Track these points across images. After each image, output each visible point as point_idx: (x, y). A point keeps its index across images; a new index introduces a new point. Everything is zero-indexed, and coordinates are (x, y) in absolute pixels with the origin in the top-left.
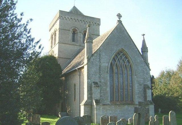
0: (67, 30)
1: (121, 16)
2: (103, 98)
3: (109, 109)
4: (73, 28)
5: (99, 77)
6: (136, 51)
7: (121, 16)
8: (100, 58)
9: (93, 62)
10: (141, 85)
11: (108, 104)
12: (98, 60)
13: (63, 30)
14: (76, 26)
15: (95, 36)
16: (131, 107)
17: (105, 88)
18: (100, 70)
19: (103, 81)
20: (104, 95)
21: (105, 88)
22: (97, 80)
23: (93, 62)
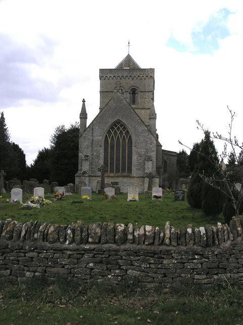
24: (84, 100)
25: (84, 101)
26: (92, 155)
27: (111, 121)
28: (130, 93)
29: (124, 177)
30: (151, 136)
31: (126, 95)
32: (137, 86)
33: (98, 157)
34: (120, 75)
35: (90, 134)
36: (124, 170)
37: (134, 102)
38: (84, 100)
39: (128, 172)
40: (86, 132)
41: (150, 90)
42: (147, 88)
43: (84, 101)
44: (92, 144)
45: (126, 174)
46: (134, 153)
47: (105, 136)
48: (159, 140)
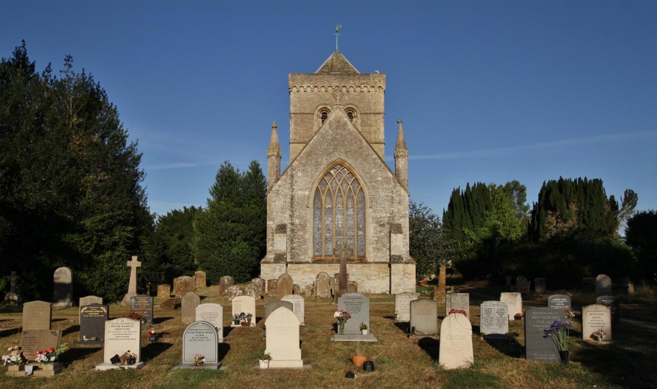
0: (307, 114)
1: (117, 356)
2: (298, 251)
3: (308, 270)
4: (320, 107)
5: (291, 216)
6: (374, 160)
7: (117, 356)
8: (292, 182)
9: (278, 191)
10: (383, 225)
11: (308, 263)
12: (288, 186)
13: (298, 116)
14: (327, 102)
15: (107, 308)
16: (356, 268)
17: (301, 233)
18: (292, 203)
19: (297, 221)
20: (300, 246)
21: (301, 233)
22: (287, 221)
23: (278, 191)
30: (399, 188)
32: (356, 103)
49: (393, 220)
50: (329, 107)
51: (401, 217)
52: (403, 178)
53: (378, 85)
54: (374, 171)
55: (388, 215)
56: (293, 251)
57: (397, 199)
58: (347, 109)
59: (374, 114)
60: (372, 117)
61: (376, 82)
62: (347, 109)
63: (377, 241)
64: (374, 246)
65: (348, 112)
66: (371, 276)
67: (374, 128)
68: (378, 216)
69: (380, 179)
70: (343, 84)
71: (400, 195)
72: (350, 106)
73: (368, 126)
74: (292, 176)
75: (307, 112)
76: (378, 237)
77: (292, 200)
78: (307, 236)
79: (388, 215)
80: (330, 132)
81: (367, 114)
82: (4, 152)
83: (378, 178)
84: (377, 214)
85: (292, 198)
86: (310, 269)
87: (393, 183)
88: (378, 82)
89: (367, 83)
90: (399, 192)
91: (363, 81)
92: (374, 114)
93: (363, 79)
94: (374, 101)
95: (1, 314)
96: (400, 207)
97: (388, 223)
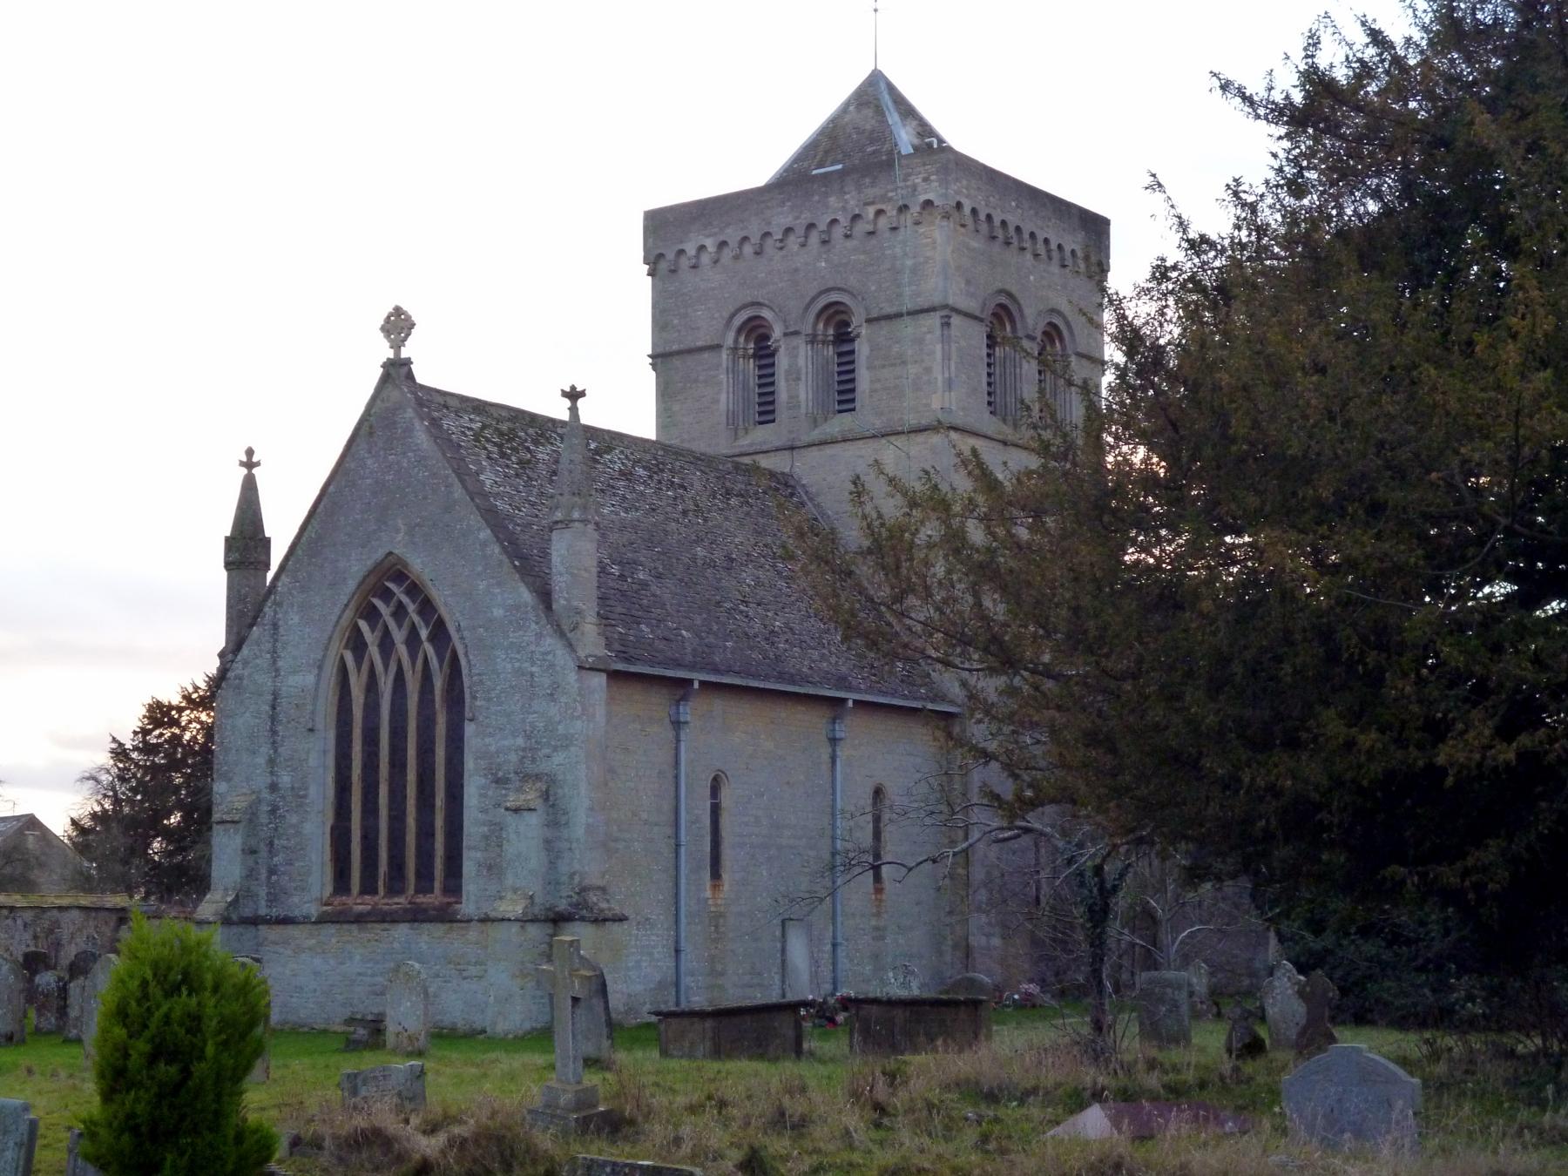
5: (272, 762)
11: (305, 920)
19: (285, 779)
24: (250, 452)
25: (250, 464)
26: (273, 787)
27: (356, 566)
28: (813, 340)
29: (416, 916)
30: (551, 642)
31: (793, 355)
32: (853, 281)
33: (299, 793)
34: (755, 230)
35: (264, 661)
36: (425, 875)
37: (845, 395)
38: (250, 452)
39: (447, 890)
40: (245, 651)
41: (922, 302)
42: (907, 291)
43: (250, 464)
44: (273, 719)
45: (435, 898)
46: (469, 763)
47: (331, 670)
48: (220, 641)
49: (534, 760)
50: (766, 313)
51: (555, 749)
52: (563, 602)
53: (922, 198)
54: (482, 585)
55: (520, 741)
56: (274, 878)
57: (546, 681)
58: (831, 311)
59: (909, 313)
60: (908, 328)
61: (915, 188)
62: (831, 311)
63: (486, 837)
64: (479, 855)
65: (839, 318)
66: (469, 963)
67: (913, 370)
68: (493, 749)
69: (498, 612)
70: (806, 217)
71: (552, 665)
72: (834, 297)
73: (894, 365)
74: (275, 626)
75: (700, 344)
76: (491, 823)
77: (274, 707)
78: (308, 828)
79: (520, 741)
80: (369, 462)
81: (888, 317)
82: (782, 517)
83: (495, 610)
84: (487, 740)
85: (276, 695)
86: (314, 941)
87: (533, 626)
88: (922, 186)
89: (885, 199)
90: (550, 657)
91: (871, 192)
92: (909, 313)
93: (873, 185)
94: (909, 263)
95: (2, 1050)
96: (553, 711)
97: (516, 773)
